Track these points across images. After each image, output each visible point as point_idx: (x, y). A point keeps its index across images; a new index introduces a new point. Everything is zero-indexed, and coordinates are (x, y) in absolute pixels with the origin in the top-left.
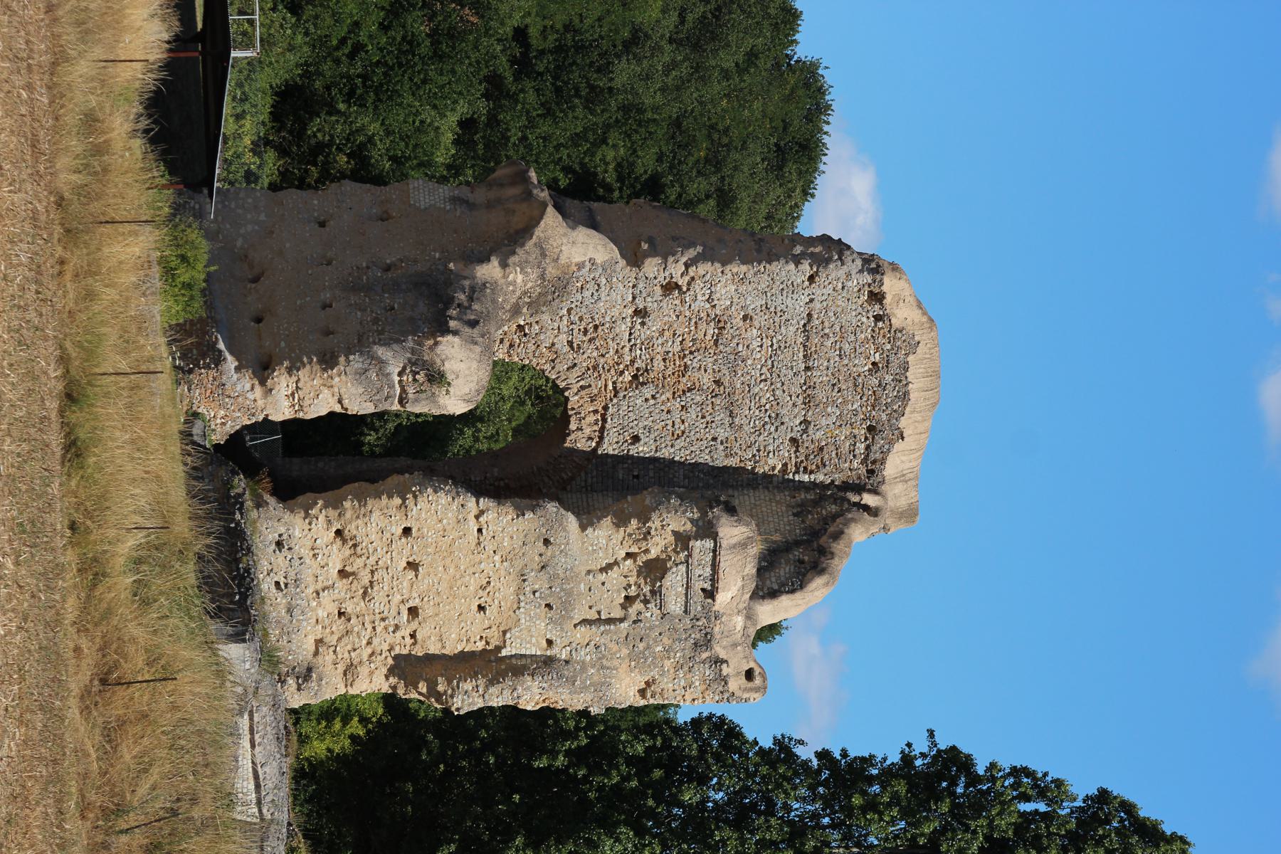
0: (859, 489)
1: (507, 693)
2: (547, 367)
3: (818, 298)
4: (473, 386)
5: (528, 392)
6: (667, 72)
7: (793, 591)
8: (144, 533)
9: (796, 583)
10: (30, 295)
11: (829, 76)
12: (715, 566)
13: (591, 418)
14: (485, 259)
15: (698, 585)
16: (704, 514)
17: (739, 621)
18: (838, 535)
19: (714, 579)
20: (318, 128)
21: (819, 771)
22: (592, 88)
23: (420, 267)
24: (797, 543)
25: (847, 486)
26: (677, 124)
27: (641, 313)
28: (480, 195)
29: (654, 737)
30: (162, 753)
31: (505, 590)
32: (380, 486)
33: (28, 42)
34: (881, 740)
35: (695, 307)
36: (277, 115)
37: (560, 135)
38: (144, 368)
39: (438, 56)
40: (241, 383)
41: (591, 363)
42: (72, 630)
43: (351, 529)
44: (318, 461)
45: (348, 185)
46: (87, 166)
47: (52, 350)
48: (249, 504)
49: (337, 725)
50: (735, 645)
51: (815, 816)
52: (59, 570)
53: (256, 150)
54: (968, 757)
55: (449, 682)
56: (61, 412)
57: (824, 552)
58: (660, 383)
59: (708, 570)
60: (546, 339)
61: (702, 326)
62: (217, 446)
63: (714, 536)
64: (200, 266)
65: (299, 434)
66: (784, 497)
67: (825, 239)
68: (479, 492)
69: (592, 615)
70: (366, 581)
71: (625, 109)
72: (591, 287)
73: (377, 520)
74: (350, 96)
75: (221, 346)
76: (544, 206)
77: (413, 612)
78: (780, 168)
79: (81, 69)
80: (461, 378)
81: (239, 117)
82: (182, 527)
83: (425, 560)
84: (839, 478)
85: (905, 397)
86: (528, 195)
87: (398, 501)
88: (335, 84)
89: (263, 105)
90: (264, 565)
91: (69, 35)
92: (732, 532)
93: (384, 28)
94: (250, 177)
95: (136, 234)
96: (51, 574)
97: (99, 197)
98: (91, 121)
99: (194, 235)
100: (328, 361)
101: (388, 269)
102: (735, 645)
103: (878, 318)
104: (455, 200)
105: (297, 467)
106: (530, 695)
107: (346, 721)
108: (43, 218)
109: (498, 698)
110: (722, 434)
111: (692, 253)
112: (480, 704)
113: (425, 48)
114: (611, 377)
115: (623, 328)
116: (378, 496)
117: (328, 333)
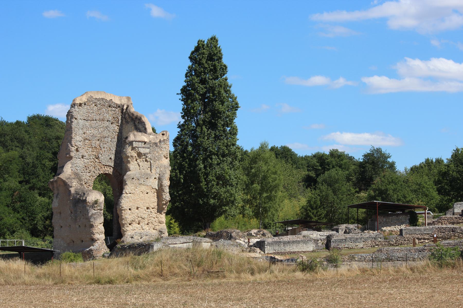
0: (123, 109)
1: (166, 188)
2: (94, 178)
3: (80, 117)
4: (98, 194)
5: (100, 182)
7: (145, 125)
9: (143, 124)
10: (76, 291)
11: (31, 115)
12: (139, 142)
13: (106, 168)
14: (70, 191)
15: (143, 145)
16: (127, 144)
17: (151, 136)
18: (133, 114)
19: (142, 142)
20: (40, 227)
22: (32, 167)
23: (71, 206)
24: (134, 123)
25: (122, 112)
26: (41, 148)
28: (56, 192)
31: (143, 188)
32: (120, 215)
36: (37, 236)
39: (25, 201)
41: (93, 168)
42: (150, 282)
43: (129, 222)
44: (114, 229)
46: (48, 278)
47: (89, 286)
48: (123, 244)
49: (172, 225)
50: (157, 137)
52: (137, 285)
53: (45, 241)
55: (163, 201)
56: (102, 284)
57: (136, 118)
58: (98, 153)
61: (86, 143)
62: (110, 251)
63: (133, 141)
64: (71, 254)
66: (124, 126)
67: (67, 116)
68: (121, 193)
69: (149, 169)
70: (141, 219)
71: (37, 159)
72: (77, 168)
73: (127, 216)
75: (88, 249)
76: (58, 178)
77: (148, 208)
78: (51, 126)
79: (27, 278)
80: (96, 197)
81: (37, 245)
82: (128, 258)
83: (136, 205)
84: (120, 114)
85: (103, 99)
86: (56, 181)
87: (123, 211)
89: (35, 239)
90: (137, 241)
91: (19, 281)
92: (131, 138)
93: (18, 212)
94: (51, 242)
96: (138, 287)
98: (38, 277)
99: (64, 255)
100: (92, 226)
101: (72, 212)
102: (157, 137)
103: (85, 104)
104: (57, 197)
105: (115, 234)
106: (167, 183)
107: (171, 224)
109: (167, 190)
110: (110, 139)
111: (70, 145)
112: (168, 194)
113: (23, 203)
115: (86, 161)
117: (86, 226)
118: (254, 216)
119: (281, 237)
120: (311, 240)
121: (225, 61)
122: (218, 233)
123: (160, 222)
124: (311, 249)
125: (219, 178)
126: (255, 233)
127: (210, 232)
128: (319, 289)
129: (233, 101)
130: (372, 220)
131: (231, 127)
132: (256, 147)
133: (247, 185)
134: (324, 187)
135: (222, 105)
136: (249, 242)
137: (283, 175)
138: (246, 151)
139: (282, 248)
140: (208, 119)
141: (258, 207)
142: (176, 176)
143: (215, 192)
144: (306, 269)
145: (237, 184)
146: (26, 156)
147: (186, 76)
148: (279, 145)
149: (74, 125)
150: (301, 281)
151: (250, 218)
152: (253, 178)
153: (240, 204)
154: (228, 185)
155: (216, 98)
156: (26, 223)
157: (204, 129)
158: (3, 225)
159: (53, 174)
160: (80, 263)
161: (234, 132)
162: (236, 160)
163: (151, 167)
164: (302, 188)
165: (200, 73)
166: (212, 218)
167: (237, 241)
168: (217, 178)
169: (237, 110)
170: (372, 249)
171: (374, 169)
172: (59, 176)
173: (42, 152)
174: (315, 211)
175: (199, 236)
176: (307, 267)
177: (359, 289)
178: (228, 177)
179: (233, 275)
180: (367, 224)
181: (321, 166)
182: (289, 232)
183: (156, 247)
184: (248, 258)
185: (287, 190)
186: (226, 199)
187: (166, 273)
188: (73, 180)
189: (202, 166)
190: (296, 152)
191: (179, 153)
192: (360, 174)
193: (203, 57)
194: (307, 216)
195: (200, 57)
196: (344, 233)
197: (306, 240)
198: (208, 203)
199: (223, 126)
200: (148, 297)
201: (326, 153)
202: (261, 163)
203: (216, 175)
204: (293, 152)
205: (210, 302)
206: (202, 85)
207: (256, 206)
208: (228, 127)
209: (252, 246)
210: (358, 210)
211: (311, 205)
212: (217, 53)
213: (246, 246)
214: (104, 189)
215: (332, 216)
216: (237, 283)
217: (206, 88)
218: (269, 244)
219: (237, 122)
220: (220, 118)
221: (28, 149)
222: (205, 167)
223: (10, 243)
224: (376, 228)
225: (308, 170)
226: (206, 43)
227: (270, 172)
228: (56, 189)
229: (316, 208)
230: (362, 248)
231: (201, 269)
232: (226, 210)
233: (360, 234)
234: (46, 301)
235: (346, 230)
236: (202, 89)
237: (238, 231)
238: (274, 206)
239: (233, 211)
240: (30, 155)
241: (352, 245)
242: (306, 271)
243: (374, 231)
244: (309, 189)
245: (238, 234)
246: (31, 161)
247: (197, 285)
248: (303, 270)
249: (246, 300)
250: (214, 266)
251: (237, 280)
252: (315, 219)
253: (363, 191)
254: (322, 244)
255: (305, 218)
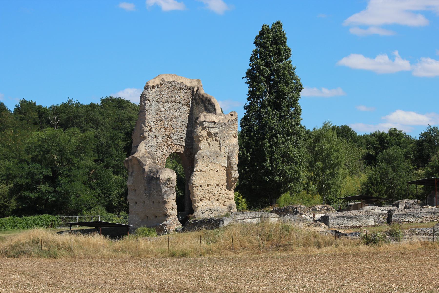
1: (235, 166)
2: (167, 156)
3: (153, 99)
4: (171, 172)
5: (171, 161)
6: (103, 131)
7: (215, 106)
8: (202, 241)
9: (213, 105)
10: (153, 263)
11: (104, 97)
12: (209, 122)
13: (177, 147)
14: (144, 169)
15: (213, 125)
16: (198, 124)
17: (221, 117)
18: (203, 96)
19: (212, 122)
20: (115, 204)
21: (251, 101)
22: (106, 146)
23: (145, 183)
24: (204, 105)
25: (193, 94)
26: (114, 129)
27: (156, 137)
28: (130, 170)
29: (244, 135)
30: (247, 237)
31: (213, 166)
32: (191, 192)
33: (100, 263)
34: (244, 89)
35: (155, 125)
36: (113, 212)
37: (116, 153)
38: (167, 240)
39: (100, 178)
40: (169, 220)
41: (166, 147)
42: (222, 256)
43: (200, 198)
44: (186, 205)
45: (128, 198)
46: (125, 252)
47: (163, 259)
48: (194, 219)
49: (240, 201)
50: (226, 118)
51: (260, 102)
52: (209, 258)
53: (119, 217)
54: (248, 70)
55: (232, 178)
56: (176, 257)
57: (206, 99)
58: (170, 133)
59: (210, 123)
60: (161, 157)
61: (159, 124)
62: (182, 226)
63: (203, 122)
64: (145, 229)
65: (180, 209)
66: (195, 107)
67: (141, 98)
68: (192, 171)
69: (219, 148)
70: (211, 195)
71: (111, 139)
72: (150, 147)
73: (198, 192)
74: (109, 197)
75: (161, 224)
76: (133, 157)
77: (217, 185)
78: (123, 107)
79: (105, 252)
80: (169, 174)
81: (113, 220)
82: (200, 233)
83: (207, 183)
84: (191, 96)
85: (174, 82)
86: (131, 160)
87: (194, 188)
88: (106, 200)
89: (110, 215)
90: (207, 216)
91: (98, 254)
92: (202, 118)
93: (95, 190)
94: (125, 218)
95: (139, 242)
96: (211, 260)
97: (132, 249)
98: (116, 250)
99: (139, 229)
100: (165, 202)
101: (146, 189)
102: (226, 118)
103: (158, 87)
104: (131, 175)
105: (187, 209)
106: (235, 161)
107: (239, 200)
108: (136, 261)
109: (236, 168)
110: (181, 120)
111: (143, 126)
112: (237, 172)
113: (99, 181)
114: (169, 143)
115: (159, 140)
116: (193, 192)
117: (159, 202)
118: (318, 192)
119: (344, 212)
120: (372, 215)
121: (289, 44)
122: (285, 208)
123: (230, 199)
124: (373, 224)
125: (284, 156)
126: (319, 208)
127: (277, 207)
128: (383, 261)
129: (297, 83)
130: (430, 196)
131: (296, 107)
132: (320, 126)
133: (311, 163)
134: (384, 165)
135: (287, 87)
136: (314, 217)
137: (344, 154)
138: (309, 130)
139: (346, 223)
140: (273, 100)
141: (321, 183)
142: (243, 153)
143: (280, 169)
144: (370, 242)
145: (301, 162)
146: (100, 136)
147: (251, 60)
148: (339, 124)
149: (147, 106)
150: (366, 254)
151: (314, 194)
152: (316, 156)
153: (304, 181)
154: (292, 162)
155: (281, 80)
156: (101, 199)
157: (269, 109)
158: (80, 201)
159: (126, 153)
160: (154, 237)
161: (298, 112)
162: (300, 139)
163: (220, 146)
164: (363, 165)
165: (266, 56)
166: (278, 194)
167: (303, 216)
168: (282, 157)
169: (300, 91)
170: (431, 223)
171: (431, 147)
172: (134, 155)
173: (115, 132)
174: (376, 188)
175: (266, 211)
176: (370, 241)
177: (422, 262)
178: (293, 155)
179: (300, 249)
180: (425, 199)
181: (380, 144)
182: (352, 208)
183: (226, 222)
184: (315, 232)
185: (349, 167)
186: (290, 176)
187: (237, 246)
188: (147, 159)
189: (268, 145)
190: (356, 131)
191: (246, 133)
192: (418, 152)
193: (268, 41)
194: (368, 192)
195: (265, 40)
196: (405, 208)
197: (368, 215)
198: (273, 179)
199: (288, 106)
200: (222, 270)
201: (385, 132)
202: (324, 141)
203: (281, 153)
204: (353, 131)
205: (281, 274)
206: (267, 67)
207: (320, 183)
208: (292, 107)
209: (316, 221)
210: (417, 186)
211: (371, 181)
212: (281, 37)
213: (311, 220)
214: (176, 166)
215: (391, 192)
216: (305, 256)
217: (271, 70)
218: (333, 219)
219: (301, 102)
220: (285, 99)
221: (102, 130)
222: (271, 146)
223: (87, 219)
224: (435, 204)
225: (367, 149)
226: (270, 27)
227: (332, 150)
228: (130, 168)
229: (377, 185)
230: (422, 222)
231: (270, 242)
232: (291, 187)
233: (419, 209)
234: (125, 274)
235: (406, 205)
236: (267, 72)
237: (303, 206)
238: (337, 183)
239: (298, 187)
240: (104, 135)
241: (412, 219)
242: (370, 245)
243: (433, 206)
244: (369, 166)
245: (303, 209)
246: (105, 141)
247: (267, 258)
248: (367, 243)
249: (315, 272)
250: (283, 239)
251: (305, 253)
252: (375, 195)
253: (421, 168)
254: (384, 218)
255: (367, 194)
